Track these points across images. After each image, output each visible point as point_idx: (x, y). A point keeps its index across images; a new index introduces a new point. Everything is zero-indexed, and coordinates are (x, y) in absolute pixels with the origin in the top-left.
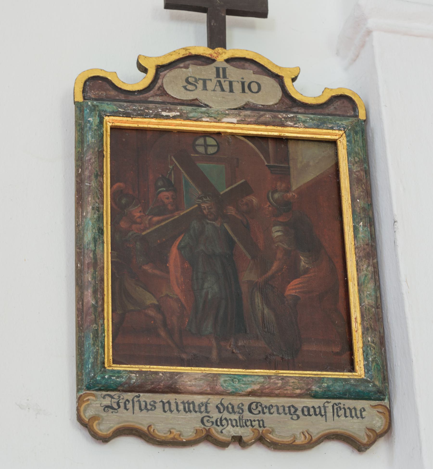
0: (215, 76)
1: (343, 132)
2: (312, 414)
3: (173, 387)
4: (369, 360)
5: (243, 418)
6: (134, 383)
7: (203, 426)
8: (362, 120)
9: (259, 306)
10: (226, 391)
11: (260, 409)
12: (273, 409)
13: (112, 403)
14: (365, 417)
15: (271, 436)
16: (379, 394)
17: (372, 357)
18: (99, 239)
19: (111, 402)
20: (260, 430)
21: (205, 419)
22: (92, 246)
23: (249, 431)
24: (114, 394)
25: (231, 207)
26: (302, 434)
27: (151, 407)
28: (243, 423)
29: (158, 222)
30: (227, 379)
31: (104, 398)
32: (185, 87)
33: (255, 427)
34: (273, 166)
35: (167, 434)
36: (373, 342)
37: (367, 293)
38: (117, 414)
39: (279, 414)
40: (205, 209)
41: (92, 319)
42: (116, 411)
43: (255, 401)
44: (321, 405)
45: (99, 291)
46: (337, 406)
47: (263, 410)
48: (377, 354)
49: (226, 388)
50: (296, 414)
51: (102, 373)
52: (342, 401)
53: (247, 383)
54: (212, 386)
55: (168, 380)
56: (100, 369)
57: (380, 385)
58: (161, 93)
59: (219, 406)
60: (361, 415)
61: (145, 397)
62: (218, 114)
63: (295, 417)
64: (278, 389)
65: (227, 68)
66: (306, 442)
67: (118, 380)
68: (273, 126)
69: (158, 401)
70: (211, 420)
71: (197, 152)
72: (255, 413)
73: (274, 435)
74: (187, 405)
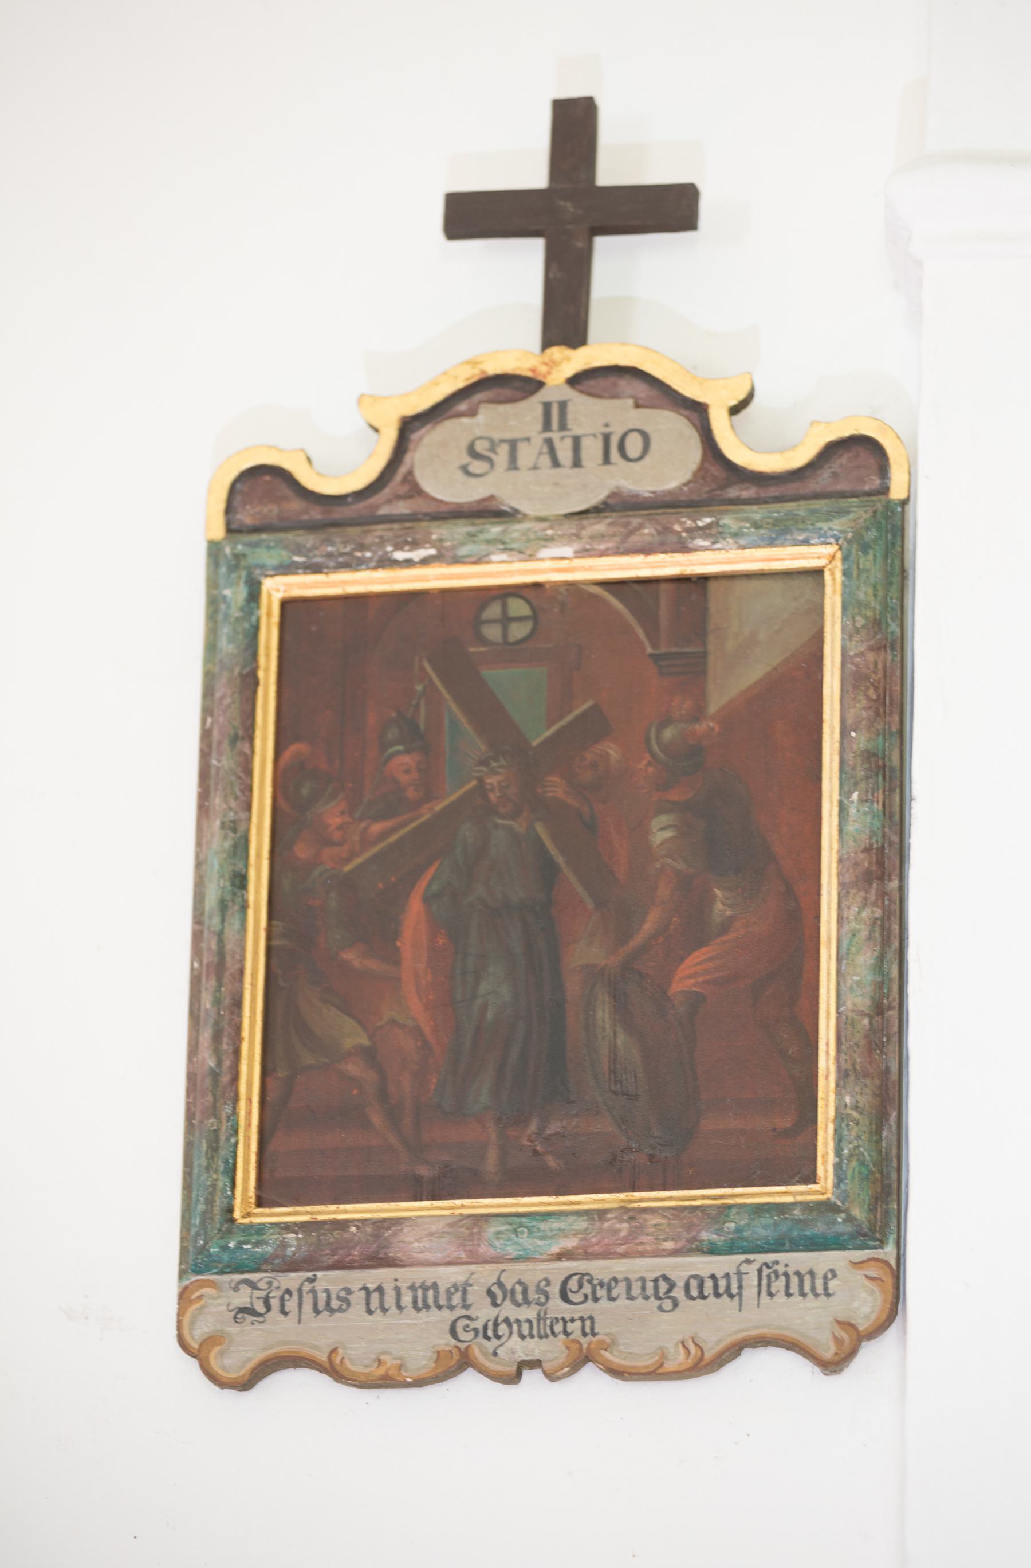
0: (539, 426)
1: (836, 547)
2: (709, 1294)
3: (381, 1256)
4: (843, 1155)
5: (548, 1316)
6: (294, 1255)
7: (453, 1342)
8: (896, 502)
9: (604, 1029)
10: (504, 1256)
11: (587, 1289)
12: (617, 1288)
13: (253, 1301)
16: (862, 1238)
17: (851, 1146)
18: (233, 901)
19: (251, 1297)
20: (584, 1341)
21: (460, 1325)
22: (216, 920)
23: (557, 1346)
24: (258, 1278)
25: (555, 779)
26: (680, 1345)
27: (340, 1303)
28: (545, 1329)
29: (384, 835)
30: (503, 1228)
31: (236, 1289)
32: (465, 470)
33: (572, 1337)
34: (665, 654)
35: (371, 1366)
36: (856, 1108)
37: (852, 979)
38: (263, 1326)
39: (631, 1298)
40: (492, 790)
41: (207, 1104)
42: (261, 1319)
43: (578, 1272)
44: (732, 1271)
45: (226, 1033)
46: (770, 1271)
47: (594, 1292)
48: (863, 1138)
49: (501, 1249)
50: (669, 1297)
51: (222, 1238)
52: (781, 1257)
53: (549, 1234)
54: (468, 1248)
55: (368, 1241)
56: (218, 1226)
57: (864, 1215)
58: (410, 491)
59: (495, 1289)
60: (826, 1288)
61: (329, 1280)
62: (528, 541)
63: (667, 1304)
64: (622, 1244)
66: (688, 1366)
67: (257, 1250)
68: (662, 553)
69: (355, 1287)
70: (473, 1325)
71: (483, 640)
72: (575, 1300)
73: (616, 1353)
74: (420, 1293)
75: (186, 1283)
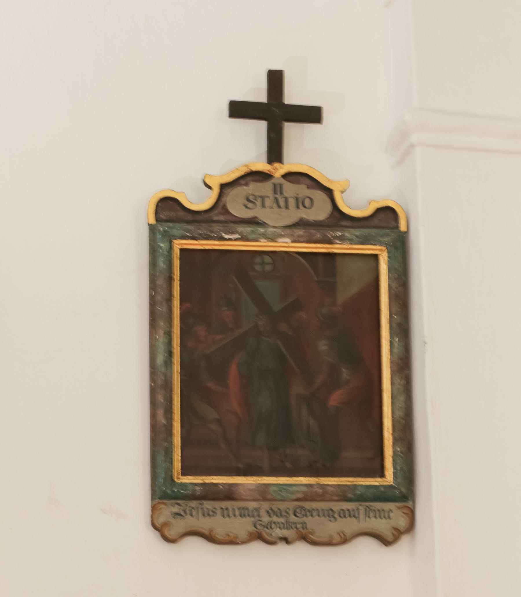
7: (256, 529)
14: (392, 518)
15: (311, 536)
22: (163, 369)
52: (371, 504)
59: (270, 511)
61: (208, 505)
65: (284, 184)
75: (155, 503)
